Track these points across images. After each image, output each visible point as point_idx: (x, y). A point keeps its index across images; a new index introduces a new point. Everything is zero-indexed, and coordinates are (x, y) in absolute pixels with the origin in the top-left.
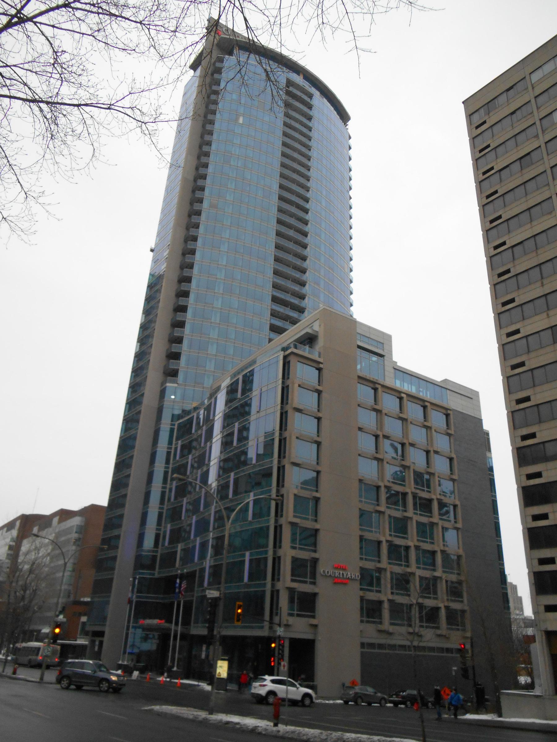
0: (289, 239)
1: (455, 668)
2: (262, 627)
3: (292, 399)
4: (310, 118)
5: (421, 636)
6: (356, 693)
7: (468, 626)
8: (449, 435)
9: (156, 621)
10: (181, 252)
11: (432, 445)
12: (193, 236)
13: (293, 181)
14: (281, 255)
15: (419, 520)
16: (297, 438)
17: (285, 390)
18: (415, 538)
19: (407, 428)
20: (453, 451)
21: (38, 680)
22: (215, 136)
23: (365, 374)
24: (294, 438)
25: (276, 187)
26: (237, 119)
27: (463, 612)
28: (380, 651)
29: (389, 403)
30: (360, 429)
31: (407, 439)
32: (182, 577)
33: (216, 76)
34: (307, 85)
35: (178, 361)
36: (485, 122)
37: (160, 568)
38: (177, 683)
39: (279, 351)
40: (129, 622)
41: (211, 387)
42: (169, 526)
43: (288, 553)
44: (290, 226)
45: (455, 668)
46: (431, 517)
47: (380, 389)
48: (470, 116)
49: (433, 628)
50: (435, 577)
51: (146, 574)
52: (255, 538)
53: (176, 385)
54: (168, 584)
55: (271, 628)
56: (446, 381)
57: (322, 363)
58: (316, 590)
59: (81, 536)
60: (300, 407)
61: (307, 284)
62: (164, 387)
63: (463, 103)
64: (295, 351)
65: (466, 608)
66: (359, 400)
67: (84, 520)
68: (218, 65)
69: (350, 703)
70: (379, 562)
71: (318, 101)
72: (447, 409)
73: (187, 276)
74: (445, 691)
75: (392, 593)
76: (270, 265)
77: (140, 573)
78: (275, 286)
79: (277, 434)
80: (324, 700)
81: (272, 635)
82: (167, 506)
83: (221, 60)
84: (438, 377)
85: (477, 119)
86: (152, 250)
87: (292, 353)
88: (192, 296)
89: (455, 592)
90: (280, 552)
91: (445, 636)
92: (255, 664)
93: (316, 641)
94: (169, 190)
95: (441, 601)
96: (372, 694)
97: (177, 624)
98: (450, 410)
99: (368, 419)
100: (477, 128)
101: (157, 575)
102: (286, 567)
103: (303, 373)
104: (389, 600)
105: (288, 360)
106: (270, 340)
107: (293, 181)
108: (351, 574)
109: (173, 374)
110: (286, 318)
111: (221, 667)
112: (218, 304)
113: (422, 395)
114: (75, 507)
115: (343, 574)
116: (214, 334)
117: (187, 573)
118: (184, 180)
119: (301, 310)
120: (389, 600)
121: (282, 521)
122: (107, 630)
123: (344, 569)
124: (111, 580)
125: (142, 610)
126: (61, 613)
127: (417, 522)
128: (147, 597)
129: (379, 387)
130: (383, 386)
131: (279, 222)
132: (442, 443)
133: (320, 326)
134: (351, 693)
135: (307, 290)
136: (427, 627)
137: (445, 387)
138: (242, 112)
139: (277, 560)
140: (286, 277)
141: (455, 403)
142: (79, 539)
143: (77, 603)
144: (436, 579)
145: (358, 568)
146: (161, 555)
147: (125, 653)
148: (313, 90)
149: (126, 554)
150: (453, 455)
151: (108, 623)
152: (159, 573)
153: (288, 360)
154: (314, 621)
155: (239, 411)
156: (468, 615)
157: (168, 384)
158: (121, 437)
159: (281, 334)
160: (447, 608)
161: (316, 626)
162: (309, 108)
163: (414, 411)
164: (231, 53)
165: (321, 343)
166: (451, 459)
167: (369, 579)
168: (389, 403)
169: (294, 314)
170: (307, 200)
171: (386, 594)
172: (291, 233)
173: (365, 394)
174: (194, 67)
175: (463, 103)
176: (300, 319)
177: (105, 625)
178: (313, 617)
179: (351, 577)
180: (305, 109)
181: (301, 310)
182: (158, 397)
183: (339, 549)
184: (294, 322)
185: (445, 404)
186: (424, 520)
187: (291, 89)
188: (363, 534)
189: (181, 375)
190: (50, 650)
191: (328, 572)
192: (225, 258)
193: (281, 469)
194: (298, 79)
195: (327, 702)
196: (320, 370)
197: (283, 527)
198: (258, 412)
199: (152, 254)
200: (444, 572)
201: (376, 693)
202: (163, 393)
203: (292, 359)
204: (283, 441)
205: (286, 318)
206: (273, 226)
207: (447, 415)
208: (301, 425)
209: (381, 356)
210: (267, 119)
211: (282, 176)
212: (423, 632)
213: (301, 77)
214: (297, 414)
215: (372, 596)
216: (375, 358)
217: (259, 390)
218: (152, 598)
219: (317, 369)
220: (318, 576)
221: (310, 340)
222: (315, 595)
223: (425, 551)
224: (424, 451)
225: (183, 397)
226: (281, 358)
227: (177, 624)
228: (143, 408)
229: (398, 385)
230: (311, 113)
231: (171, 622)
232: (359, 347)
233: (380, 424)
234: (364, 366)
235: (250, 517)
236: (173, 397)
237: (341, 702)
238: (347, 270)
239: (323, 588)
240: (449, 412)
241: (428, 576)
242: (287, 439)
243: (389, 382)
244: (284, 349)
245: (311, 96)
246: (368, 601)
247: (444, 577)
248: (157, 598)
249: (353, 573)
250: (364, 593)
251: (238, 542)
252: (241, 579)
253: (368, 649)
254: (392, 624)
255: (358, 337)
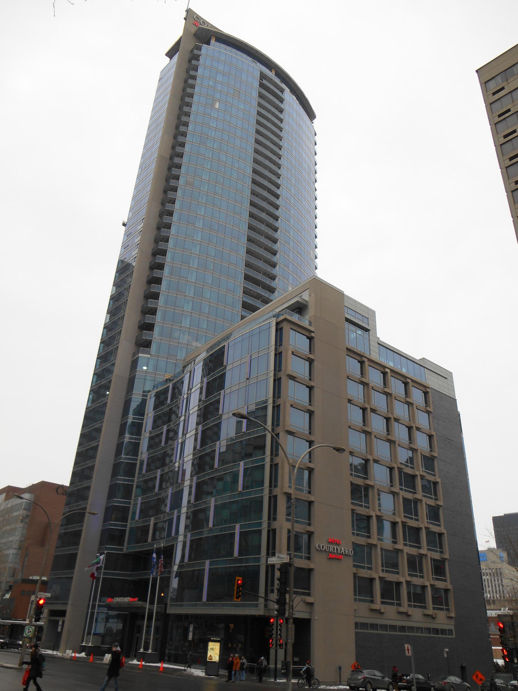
0: (262, 221)
1: (447, 650)
2: (257, 606)
3: (286, 366)
4: (281, 111)
5: (409, 616)
6: (365, 678)
7: (452, 607)
8: (428, 413)
9: (127, 599)
10: (155, 227)
11: (414, 422)
12: (168, 211)
13: (266, 167)
14: (254, 235)
15: (405, 496)
16: (291, 406)
17: (278, 355)
18: (402, 514)
19: (392, 402)
20: (432, 428)
21: (17, 666)
22: (192, 118)
23: (352, 345)
24: (288, 405)
25: (249, 171)
26: (213, 105)
27: (446, 591)
28: (373, 632)
29: (375, 377)
30: (350, 401)
31: (392, 413)
32: (159, 552)
33: (194, 62)
34: (277, 81)
35: (152, 332)
36: (503, 88)
37: (128, 544)
38: (159, 667)
39: (270, 318)
40: (95, 600)
41: (184, 360)
42: (140, 499)
43: (283, 525)
44: (262, 209)
45: (447, 650)
46: (415, 493)
47: (367, 363)
48: (485, 84)
49: (421, 607)
50: (421, 554)
51: (112, 548)
52: (250, 509)
53: (149, 356)
54: (141, 560)
55: (266, 606)
56: (423, 359)
57: (313, 332)
58: (312, 566)
59: (29, 513)
60: (294, 374)
61: (278, 266)
62: (137, 357)
63: (477, 71)
64: (289, 317)
65: (450, 587)
66: (348, 372)
67: (34, 495)
68: (196, 52)
69: (361, 689)
70: (369, 537)
71: (288, 95)
72: (426, 387)
73: (162, 249)
74: (477, 676)
75: (383, 570)
76: (243, 244)
77: (107, 549)
78: (248, 265)
79: (270, 401)
80: (327, 685)
81: (267, 614)
82: (138, 478)
83: (200, 49)
84: (417, 356)
85: (493, 86)
86: (124, 225)
87: (285, 320)
88: (166, 269)
89: (439, 568)
90: (275, 525)
91: (432, 616)
92: (230, 645)
93: (312, 621)
94: (144, 166)
95: (428, 580)
96: (380, 678)
97: (152, 603)
98: (429, 388)
99: (355, 391)
100: (494, 94)
101: (125, 551)
102: (282, 540)
103: (296, 341)
104: (380, 577)
105: (280, 327)
106: (243, 317)
107: (266, 167)
108: (345, 550)
109: (145, 345)
110: (258, 297)
111: (212, 649)
112: (192, 278)
113: (404, 371)
114: (23, 483)
115: (337, 548)
116: (188, 308)
117: (164, 547)
118: (161, 157)
119: (272, 290)
120: (380, 577)
121: (277, 491)
122: (69, 609)
123: (338, 544)
124: (76, 554)
125: (110, 589)
126: (7, 592)
127: (404, 499)
128: (114, 574)
129: (366, 360)
130: (370, 360)
131: (252, 204)
132: (422, 420)
133: (310, 295)
134: (360, 678)
135: (276, 271)
136: (415, 606)
137: (423, 365)
138: (218, 97)
139: (272, 533)
140: (258, 257)
141: (432, 382)
142: (28, 516)
143: (26, 581)
144: (421, 556)
145: (351, 544)
146: (131, 529)
147: (89, 633)
148: (283, 86)
149: (92, 527)
150: (433, 433)
151: (70, 602)
152: (127, 548)
153: (280, 327)
154: (309, 599)
155: (215, 384)
156: (451, 596)
157: (140, 355)
158: (87, 408)
159: (267, 304)
160: (432, 586)
161: (311, 604)
162: (280, 102)
163: (397, 387)
164: (208, 43)
165: (311, 312)
166: (430, 437)
167: (362, 554)
168: (375, 377)
169: (265, 294)
170: (278, 187)
171: (377, 572)
172: (263, 216)
173: (353, 366)
174: (170, 54)
175: (477, 71)
176: (271, 298)
177: (67, 604)
178: (309, 594)
179: (345, 552)
180: (277, 102)
181: (272, 290)
182: (130, 366)
183: (332, 522)
184: (266, 301)
185: (423, 382)
186: (409, 496)
187: (264, 82)
188: (355, 508)
189: (154, 346)
190: (31, 630)
191: (323, 546)
192: (200, 234)
193: (275, 437)
194: (271, 74)
195: (331, 688)
196: (311, 339)
197: (279, 498)
198: (247, 379)
199: (124, 228)
200: (428, 549)
201: (383, 678)
202: (134, 364)
203: (286, 326)
204: (276, 408)
205: (258, 297)
206: (246, 207)
207: (426, 393)
208: (296, 393)
209: (367, 330)
210: (241, 106)
211: (255, 161)
212: (411, 611)
213: (274, 72)
214: (291, 382)
215: (364, 573)
216: (360, 332)
217: (249, 356)
218: (118, 575)
219: (308, 338)
220: (313, 550)
221: (300, 308)
222: (310, 570)
223: (410, 528)
224: (407, 427)
225: (156, 368)
226: (274, 324)
227: (152, 603)
228: (114, 378)
229: (382, 360)
230: (282, 106)
231: (146, 601)
232: (347, 320)
233: (367, 397)
234: (353, 337)
235: (240, 488)
236: (145, 368)
237: (348, 687)
238: (313, 256)
239: (318, 563)
240: (428, 390)
241: (415, 554)
242: (281, 407)
243: (374, 356)
244: (277, 316)
245: (282, 91)
246: (360, 578)
247: (429, 555)
248: (124, 575)
249: (346, 548)
250: (356, 570)
251: (226, 514)
252: (231, 553)
253: (361, 629)
254: (383, 603)
255: (346, 308)
